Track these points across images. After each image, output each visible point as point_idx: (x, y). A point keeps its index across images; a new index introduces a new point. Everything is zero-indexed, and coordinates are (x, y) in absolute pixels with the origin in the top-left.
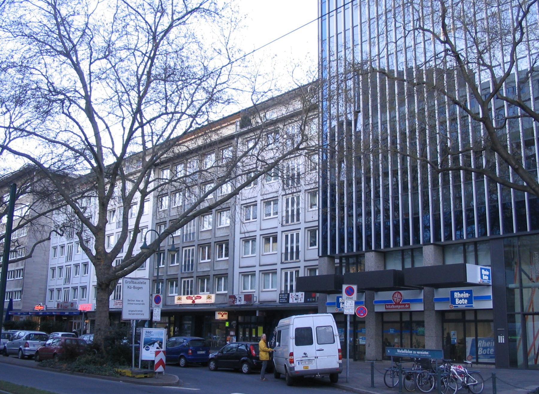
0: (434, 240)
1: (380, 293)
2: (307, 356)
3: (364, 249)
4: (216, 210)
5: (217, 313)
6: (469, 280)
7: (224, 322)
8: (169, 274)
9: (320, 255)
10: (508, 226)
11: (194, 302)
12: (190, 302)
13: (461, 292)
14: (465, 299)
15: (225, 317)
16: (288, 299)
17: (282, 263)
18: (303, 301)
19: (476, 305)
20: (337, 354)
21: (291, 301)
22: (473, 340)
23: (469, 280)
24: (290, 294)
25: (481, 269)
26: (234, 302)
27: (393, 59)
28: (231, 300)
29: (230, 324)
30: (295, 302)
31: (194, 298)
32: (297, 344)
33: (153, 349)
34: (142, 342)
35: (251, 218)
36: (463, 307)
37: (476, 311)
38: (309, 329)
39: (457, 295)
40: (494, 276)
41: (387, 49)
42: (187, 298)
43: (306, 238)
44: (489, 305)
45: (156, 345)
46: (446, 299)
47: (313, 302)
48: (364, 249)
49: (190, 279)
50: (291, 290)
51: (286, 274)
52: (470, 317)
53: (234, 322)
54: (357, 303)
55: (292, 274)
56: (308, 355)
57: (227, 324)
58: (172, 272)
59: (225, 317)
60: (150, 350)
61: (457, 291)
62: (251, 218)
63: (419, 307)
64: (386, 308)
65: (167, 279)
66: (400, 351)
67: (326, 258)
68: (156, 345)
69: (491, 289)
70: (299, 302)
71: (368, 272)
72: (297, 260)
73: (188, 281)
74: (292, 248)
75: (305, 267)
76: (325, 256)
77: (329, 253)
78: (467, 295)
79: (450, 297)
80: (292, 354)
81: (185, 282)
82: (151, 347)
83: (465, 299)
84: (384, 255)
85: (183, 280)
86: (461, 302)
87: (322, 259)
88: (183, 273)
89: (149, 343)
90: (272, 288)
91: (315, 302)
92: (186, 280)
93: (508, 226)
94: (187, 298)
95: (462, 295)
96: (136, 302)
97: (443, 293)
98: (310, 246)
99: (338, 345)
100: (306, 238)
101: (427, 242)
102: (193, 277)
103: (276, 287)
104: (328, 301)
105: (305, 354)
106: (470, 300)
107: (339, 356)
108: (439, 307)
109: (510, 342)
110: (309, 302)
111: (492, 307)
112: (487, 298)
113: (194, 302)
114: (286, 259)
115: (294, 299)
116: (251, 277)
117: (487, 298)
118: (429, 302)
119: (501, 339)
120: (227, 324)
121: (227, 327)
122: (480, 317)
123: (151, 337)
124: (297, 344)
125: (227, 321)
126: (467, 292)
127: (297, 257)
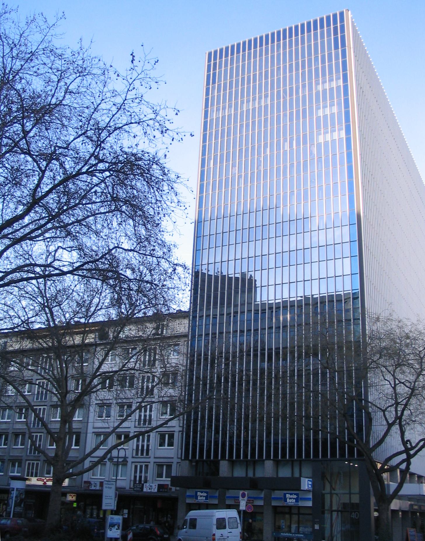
0: (274, 457)
1: (230, 491)
2: (222, 536)
3: (219, 458)
4: (157, 432)
5: (68, 495)
6: (302, 489)
7: (72, 502)
8: (11, 454)
9: (183, 458)
10: (325, 454)
11: (45, 483)
12: (41, 483)
13: (291, 494)
14: (294, 499)
15: (74, 498)
16: (142, 488)
17: (133, 457)
18: (156, 490)
19: (301, 504)
20: (239, 535)
21: (145, 490)
22: (296, 527)
23: (302, 489)
24: (145, 484)
25: (308, 480)
26: (89, 487)
27: (225, 264)
28: (87, 485)
29: (77, 505)
30: (149, 491)
31: (45, 480)
32: (217, 528)
33: (114, 529)
34: (108, 525)
35: (104, 415)
36: (292, 504)
37: (299, 507)
38: (224, 519)
39: (199, 494)
40: (313, 485)
41: (12, 65)
42: (38, 480)
43: (157, 439)
44: (310, 504)
45: (116, 527)
46: (280, 499)
47: (165, 492)
48: (219, 458)
49: (35, 462)
50: (146, 481)
51: (136, 467)
52: (294, 511)
53: (82, 503)
54: (246, 503)
55: (141, 467)
56: (224, 535)
57: (75, 505)
58: (16, 454)
59: (74, 498)
60: (113, 530)
61: (199, 492)
62: (104, 415)
63: (261, 503)
64: (235, 502)
65: (9, 460)
66: (283, 534)
67: (187, 462)
68: (116, 527)
69: (311, 493)
70: (153, 491)
71: (236, 477)
72: (147, 457)
73: (33, 464)
74: (143, 446)
75: (154, 462)
76: (187, 460)
77: (190, 458)
78: (295, 496)
79: (283, 497)
80: (214, 535)
81: (29, 464)
82: (113, 528)
83: (204, 496)
84: (232, 463)
85: (27, 462)
86: (291, 501)
87: (184, 462)
88: (29, 456)
89: (112, 525)
90: (121, 477)
91: (167, 492)
92: (31, 462)
93: (325, 454)
94: (38, 480)
95: (292, 496)
96: (109, 498)
97: (278, 494)
98: (160, 446)
99: (240, 529)
100: (157, 439)
101: (268, 457)
102: (39, 460)
103: (125, 476)
104: (188, 494)
105: (222, 535)
106: (297, 500)
107: (240, 536)
108: (274, 503)
109: (322, 529)
110: (162, 492)
111: (311, 506)
112: (261, 498)
113: (45, 483)
114: (137, 454)
115: (148, 489)
116: (341, 514)
117: (308, 499)
118: (268, 500)
119: (317, 527)
120: (75, 505)
121: (75, 508)
122: (302, 511)
123: (114, 521)
124: (217, 528)
125: (75, 502)
126: (295, 494)
127: (147, 453)
